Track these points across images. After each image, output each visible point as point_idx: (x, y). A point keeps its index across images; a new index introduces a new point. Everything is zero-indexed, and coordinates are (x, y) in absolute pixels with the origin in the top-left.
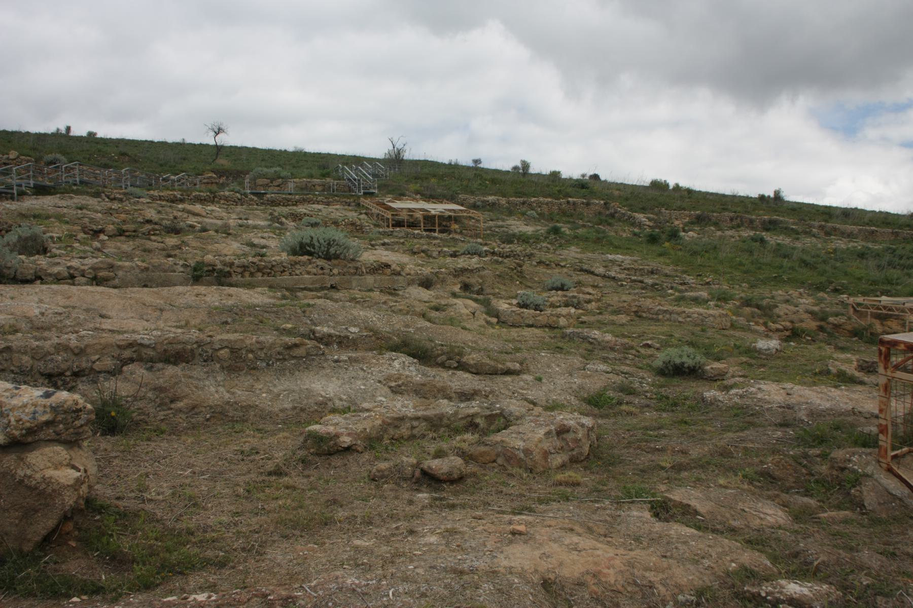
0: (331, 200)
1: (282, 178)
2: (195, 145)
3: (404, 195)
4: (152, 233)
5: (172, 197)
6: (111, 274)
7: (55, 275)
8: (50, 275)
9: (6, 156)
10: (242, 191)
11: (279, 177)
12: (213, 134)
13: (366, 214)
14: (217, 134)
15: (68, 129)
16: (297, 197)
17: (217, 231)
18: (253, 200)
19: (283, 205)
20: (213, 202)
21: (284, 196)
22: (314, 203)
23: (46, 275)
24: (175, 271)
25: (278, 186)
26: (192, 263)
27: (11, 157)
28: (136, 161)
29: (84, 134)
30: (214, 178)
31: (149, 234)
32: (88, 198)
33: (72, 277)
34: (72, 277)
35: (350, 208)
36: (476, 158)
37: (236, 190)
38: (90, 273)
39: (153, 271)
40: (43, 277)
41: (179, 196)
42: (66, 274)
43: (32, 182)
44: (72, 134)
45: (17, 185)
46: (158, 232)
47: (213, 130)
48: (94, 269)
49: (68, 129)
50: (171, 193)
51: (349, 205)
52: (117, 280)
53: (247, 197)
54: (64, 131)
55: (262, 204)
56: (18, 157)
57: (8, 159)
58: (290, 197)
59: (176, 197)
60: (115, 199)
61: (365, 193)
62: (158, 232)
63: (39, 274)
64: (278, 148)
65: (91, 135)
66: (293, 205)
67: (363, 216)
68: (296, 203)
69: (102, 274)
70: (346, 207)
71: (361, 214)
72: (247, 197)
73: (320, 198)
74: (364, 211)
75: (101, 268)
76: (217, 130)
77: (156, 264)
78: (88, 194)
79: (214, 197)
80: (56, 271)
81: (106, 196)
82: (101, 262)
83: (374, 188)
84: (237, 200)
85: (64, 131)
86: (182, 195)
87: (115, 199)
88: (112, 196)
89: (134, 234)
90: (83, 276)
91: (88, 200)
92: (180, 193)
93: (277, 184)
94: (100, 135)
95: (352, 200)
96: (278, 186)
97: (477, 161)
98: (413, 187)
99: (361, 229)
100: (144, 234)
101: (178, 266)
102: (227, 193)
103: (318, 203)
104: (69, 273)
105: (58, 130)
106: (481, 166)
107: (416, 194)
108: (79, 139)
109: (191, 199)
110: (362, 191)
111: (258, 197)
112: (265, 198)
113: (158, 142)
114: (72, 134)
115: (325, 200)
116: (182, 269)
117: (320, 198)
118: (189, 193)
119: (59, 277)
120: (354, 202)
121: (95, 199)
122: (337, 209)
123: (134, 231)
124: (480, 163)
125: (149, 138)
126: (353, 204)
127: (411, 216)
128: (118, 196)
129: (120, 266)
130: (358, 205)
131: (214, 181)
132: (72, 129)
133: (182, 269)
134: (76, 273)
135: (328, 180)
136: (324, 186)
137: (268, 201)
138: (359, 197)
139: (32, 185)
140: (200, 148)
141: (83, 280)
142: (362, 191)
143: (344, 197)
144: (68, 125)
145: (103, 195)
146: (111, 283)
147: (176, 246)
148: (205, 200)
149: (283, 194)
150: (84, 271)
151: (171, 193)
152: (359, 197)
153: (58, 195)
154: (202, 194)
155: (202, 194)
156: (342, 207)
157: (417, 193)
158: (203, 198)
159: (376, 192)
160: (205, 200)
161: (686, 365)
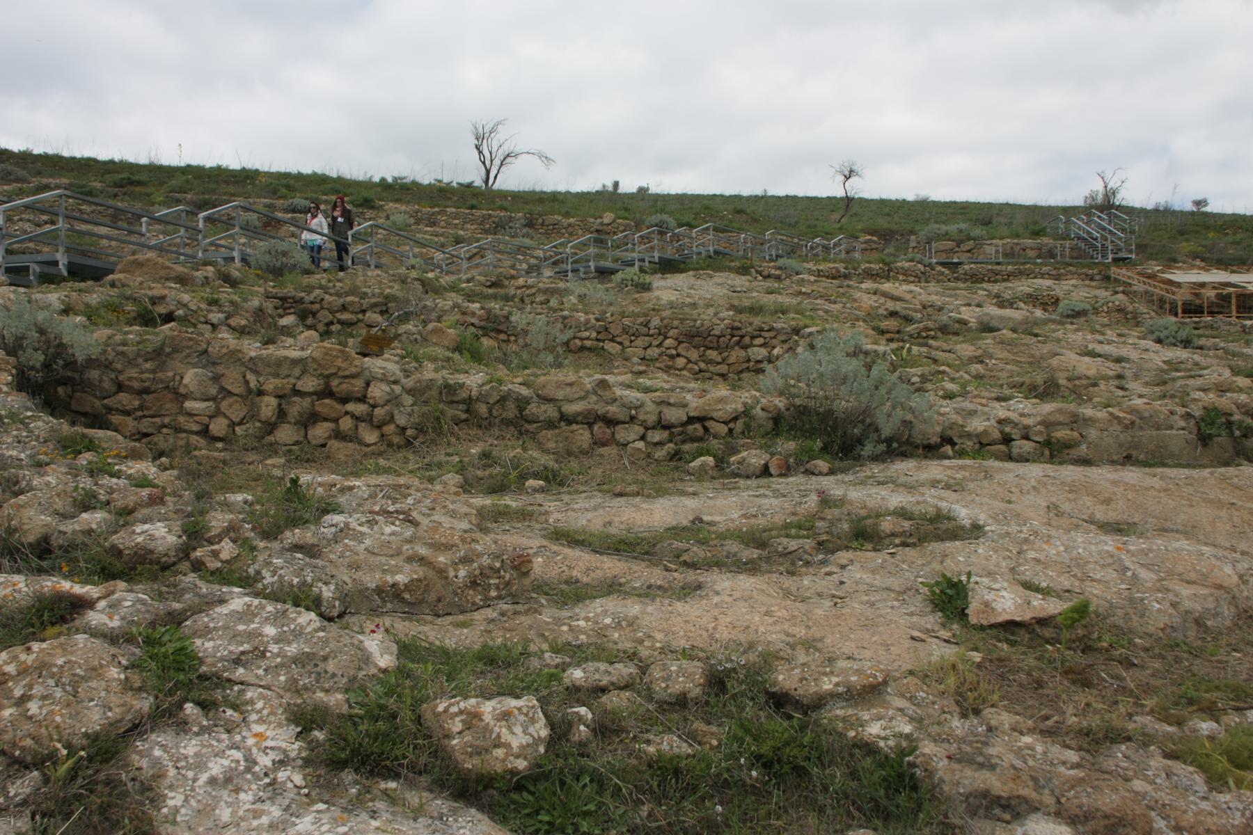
0: (1062, 271)
1: (974, 239)
2: (779, 197)
3: (1175, 260)
4: (924, 334)
5: (834, 271)
6: (1076, 434)
7: (978, 435)
8: (969, 436)
9: (599, 221)
10: (927, 260)
11: (969, 238)
12: (843, 178)
13: (1123, 292)
14: (847, 178)
15: (616, 184)
16: (1010, 268)
17: (1014, 330)
18: (942, 273)
19: (989, 281)
20: (888, 278)
21: (990, 267)
22: (1035, 278)
23: (961, 437)
24: (1171, 428)
25: (969, 251)
26: (1197, 411)
27: (606, 221)
28: (756, 221)
29: (634, 190)
30: (875, 242)
31: (919, 336)
32: (732, 275)
33: (1007, 440)
34: (1007, 440)
35: (1094, 284)
36: (1199, 198)
37: (917, 259)
38: (1041, 433)
39: (1141, 428)
40: (955, 439)
41: (842, 270)
42: (996, 435)
43: (656, 255)
44: (620, 191)
45: (639, 260)
46: (932, 333)
47: (841, 172)
48: (1048, 424)
49: (616, 184)
50: (832, 265)
51: (1091, 279)
52: (1084, 447)
53: (933, 269)
54: (610, 188)
55: (957, 279)
56: (614, 221)
57: (602, 224)
58: (999, 268)
59: (838, 271)
60: (769, 276)
61: (1116, 260)
62: (932, 333)
63: (949, 433)
64: (893, 198)
65: (642, 191)
66: (1004, 280)
67: (1120, 296)
68: (1008, 277)
69: (1061, 434)
70: (1087, 282)
71: (1116, 293)
72: (933, 269)
73: (1045, 269)
74: (1121, 289)
75: (1059, 423)
76: (847, 173)
77: (1147, 415)
78: (730, 269)
79: (890, 270)
80: (981, 429)
81: (757, 272)
82: (1060, 411)
83: (1130, 251)
84: (920, 275)
85: (610, 188)
86: (846, 268)
87: (769, 276)
88: (766, 273)
89: (897, 336)
90: (1026, 437)
91: (734, 280)
92: (844, 265)
93: (968, 248)
94: (654, 190)
95: (1095, 271)
96: (969, 251)
97: (1198, 203)
98: (1185, 246)
99: (1135, 318)
100: (911, 336)
101: (1176, 417)
102: (907, 265)
103: (1042, 276)
104: (1002, 432)
105: (604, 186)
106: (1208, 209)
107: (1194, 259)
108: (631, 196)
109: (859, 274)
110: (1110, 256)
111: (949, 269)
112: (961, 271)
113: (731, 196)
114: (620, 191)
115: (1054, 272)
116: (1182, 424)
117: (1045, 269)
118: (856, 265)
119: (985, 441)
120: (1100, 274)
121: (743, 278)
122: (1075, 286)
123: (898, 332)
124: (1205, 206)
125: (717, 191)
126: (1098, 277)
127: (1196, 295)
128: (773, 271)
129: (1090, 419)
130: (1107, 278)
131: (874, 246)
132: (621, 185)
133: (1182, 424)
134: (1016, 434)
135: (1045, 240)
136: (1040, 249)
137: (965, 274)
138: (1108, 266)
139: (656, 260)
140: (830, 204)
141: (1027, 446)
142: (1110, 256)
143: (1083, 266)
144: (616, 179)
145: (753, 270)
146: (1074, 453)
147: (976, 357)
148: (877, 275)
149: (987, 263)
150: (1027, 427)
151: (832, 265)
152: (1108, 266)
153: (691, 273)
154: (872, 266)
155: (872, 266)
156: (1080, 282)
157: (1195, 256)
158: (874, 272)
159: (1134, 257)
160: (877, 275)
161: (758, 411)
